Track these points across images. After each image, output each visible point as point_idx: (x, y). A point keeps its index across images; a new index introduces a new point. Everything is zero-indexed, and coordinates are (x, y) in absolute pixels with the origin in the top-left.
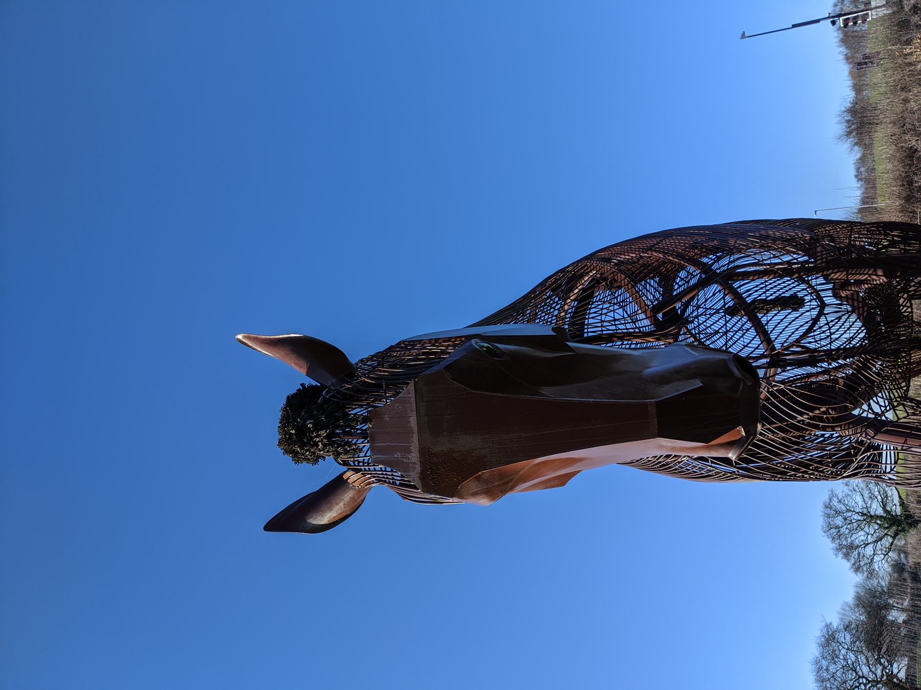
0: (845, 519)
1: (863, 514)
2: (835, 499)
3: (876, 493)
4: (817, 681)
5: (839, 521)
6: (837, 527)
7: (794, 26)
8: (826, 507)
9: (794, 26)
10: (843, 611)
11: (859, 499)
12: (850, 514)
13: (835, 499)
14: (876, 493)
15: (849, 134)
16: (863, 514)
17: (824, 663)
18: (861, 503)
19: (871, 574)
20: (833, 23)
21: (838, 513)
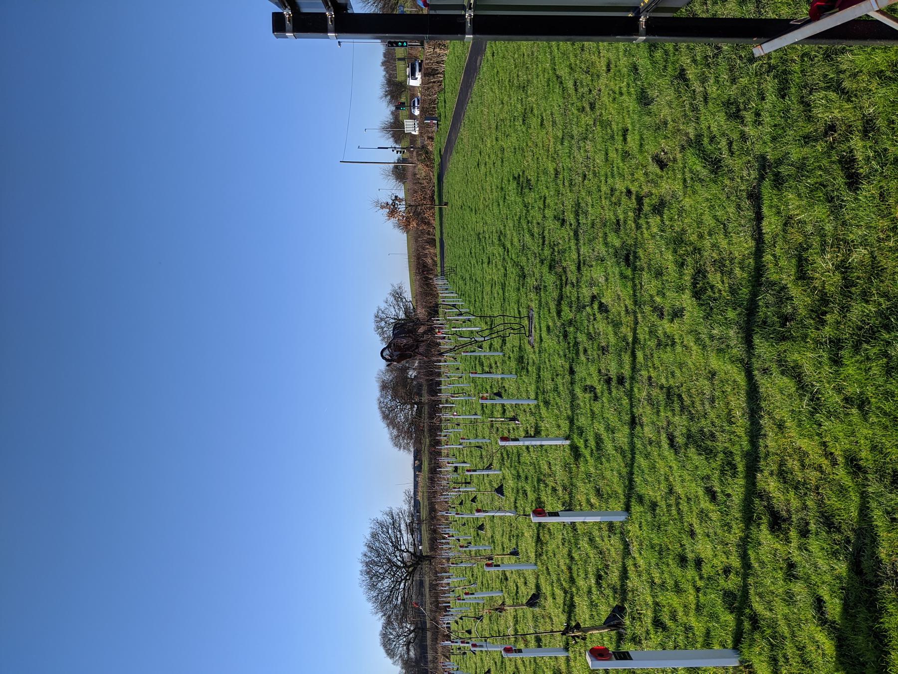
0: (386, 323)
1: (395, 319)
2: (380, 311)
3: (402, 306)
4: (379, 408)
5: (383, 324)
6: (382, 328)
7: (379, 148)
8: (376, 317)
9: (379, 148)
10: (378, 376)
11: (393, 310)
12: (388, 319)
13: (380, 311)
14: (402, 306)
15: (386, 96)
16: (395, 319)
17: (382, 399)
18: (394, 313)
19: (781, 569)
20: (393, 151)
21: (382, 319)
